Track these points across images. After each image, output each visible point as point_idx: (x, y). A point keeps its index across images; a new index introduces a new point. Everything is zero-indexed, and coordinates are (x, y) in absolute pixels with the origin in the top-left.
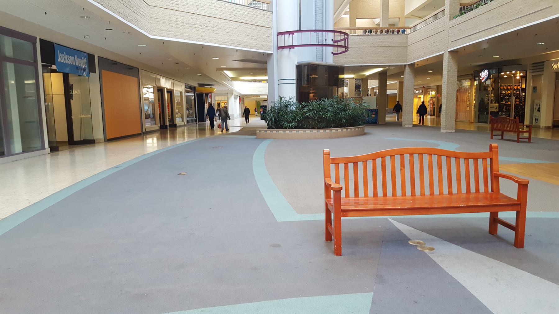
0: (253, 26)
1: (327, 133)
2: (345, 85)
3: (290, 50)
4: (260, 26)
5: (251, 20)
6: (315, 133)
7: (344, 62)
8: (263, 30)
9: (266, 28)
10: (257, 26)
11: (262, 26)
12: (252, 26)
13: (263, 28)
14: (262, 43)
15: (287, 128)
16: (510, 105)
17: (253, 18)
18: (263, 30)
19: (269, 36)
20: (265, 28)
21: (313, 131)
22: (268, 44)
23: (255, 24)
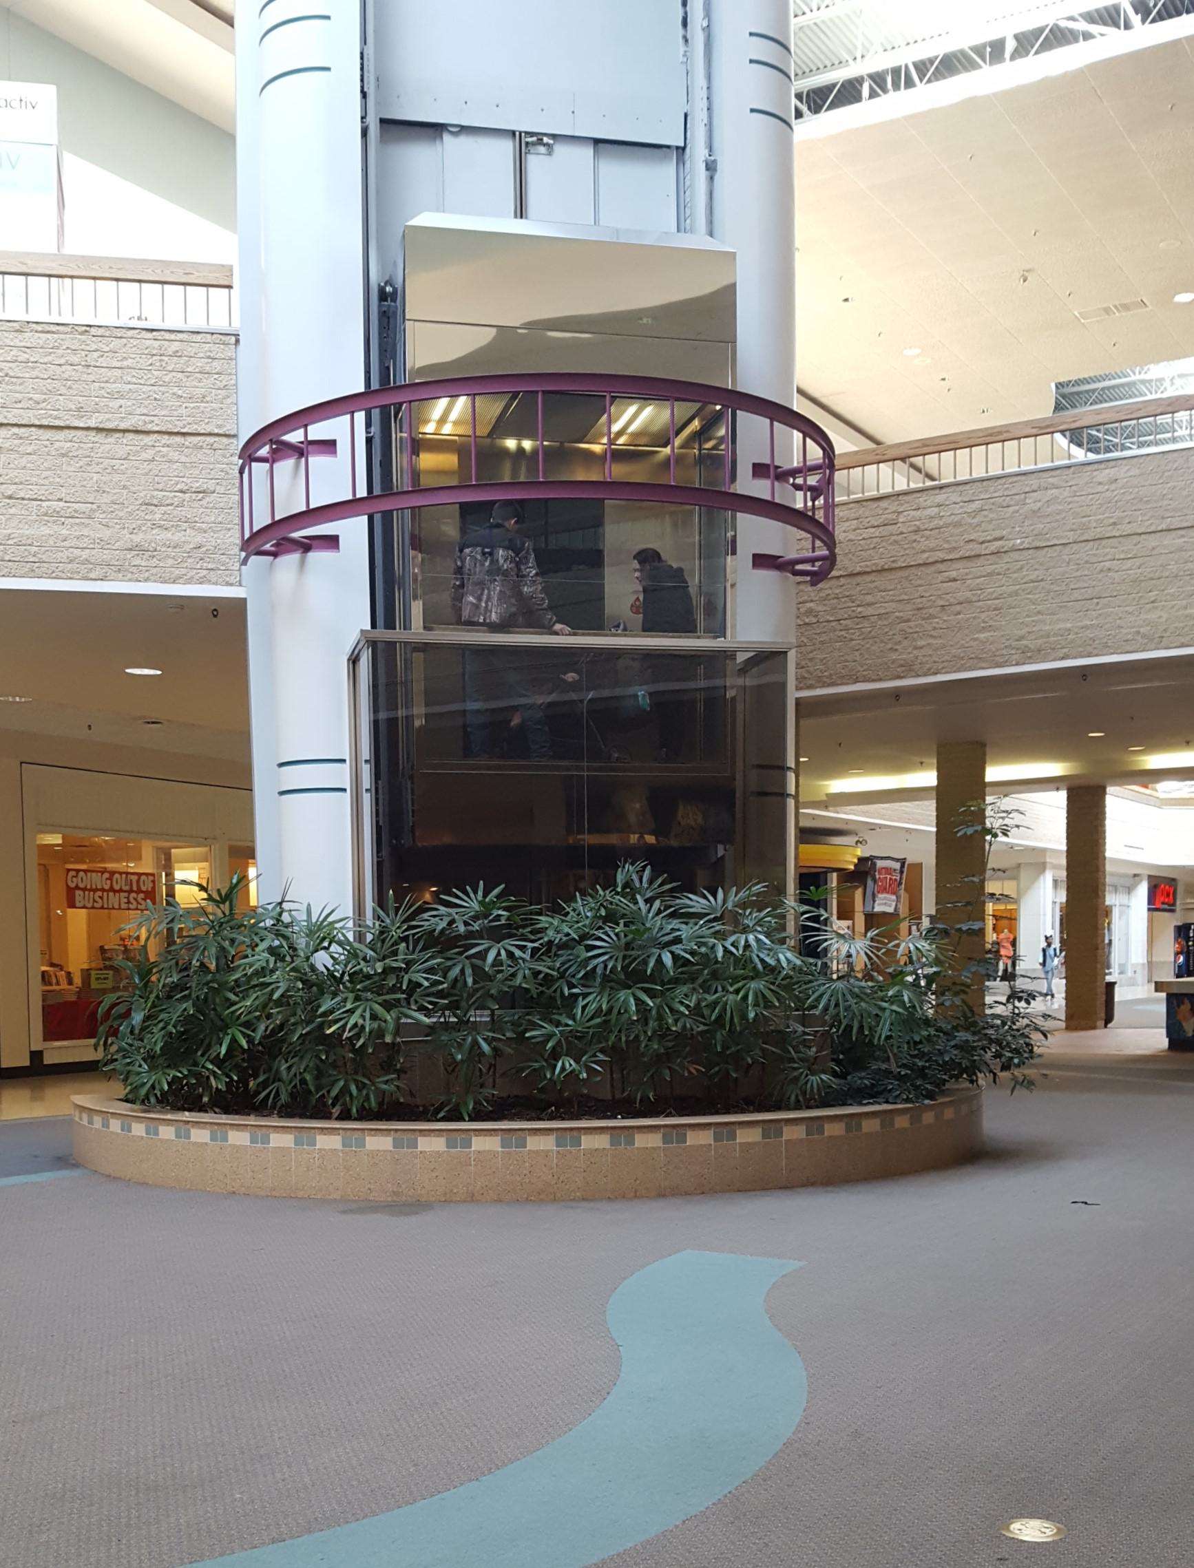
0: (61, 435)
1: (373, 1154)
2: (988, 790)
3: (302, 563)
4: (125, 431)
5: (37, 397)
6: (284, 1151)
7: (1144, 636)
8: (149, 454)
9: (179, 439)
10: (99, 430)
11: (137, 432)
12: (49, 434)
13: (148, 440)
14: (137, 538)
15: (467, 1119)
16: (496, 897)
17: (57, 384)
18: (149, 454)
19: (211, 485)
20: (165, 439)
21: (474, 1139)
22: (199, 539)
23: (76, 423)
